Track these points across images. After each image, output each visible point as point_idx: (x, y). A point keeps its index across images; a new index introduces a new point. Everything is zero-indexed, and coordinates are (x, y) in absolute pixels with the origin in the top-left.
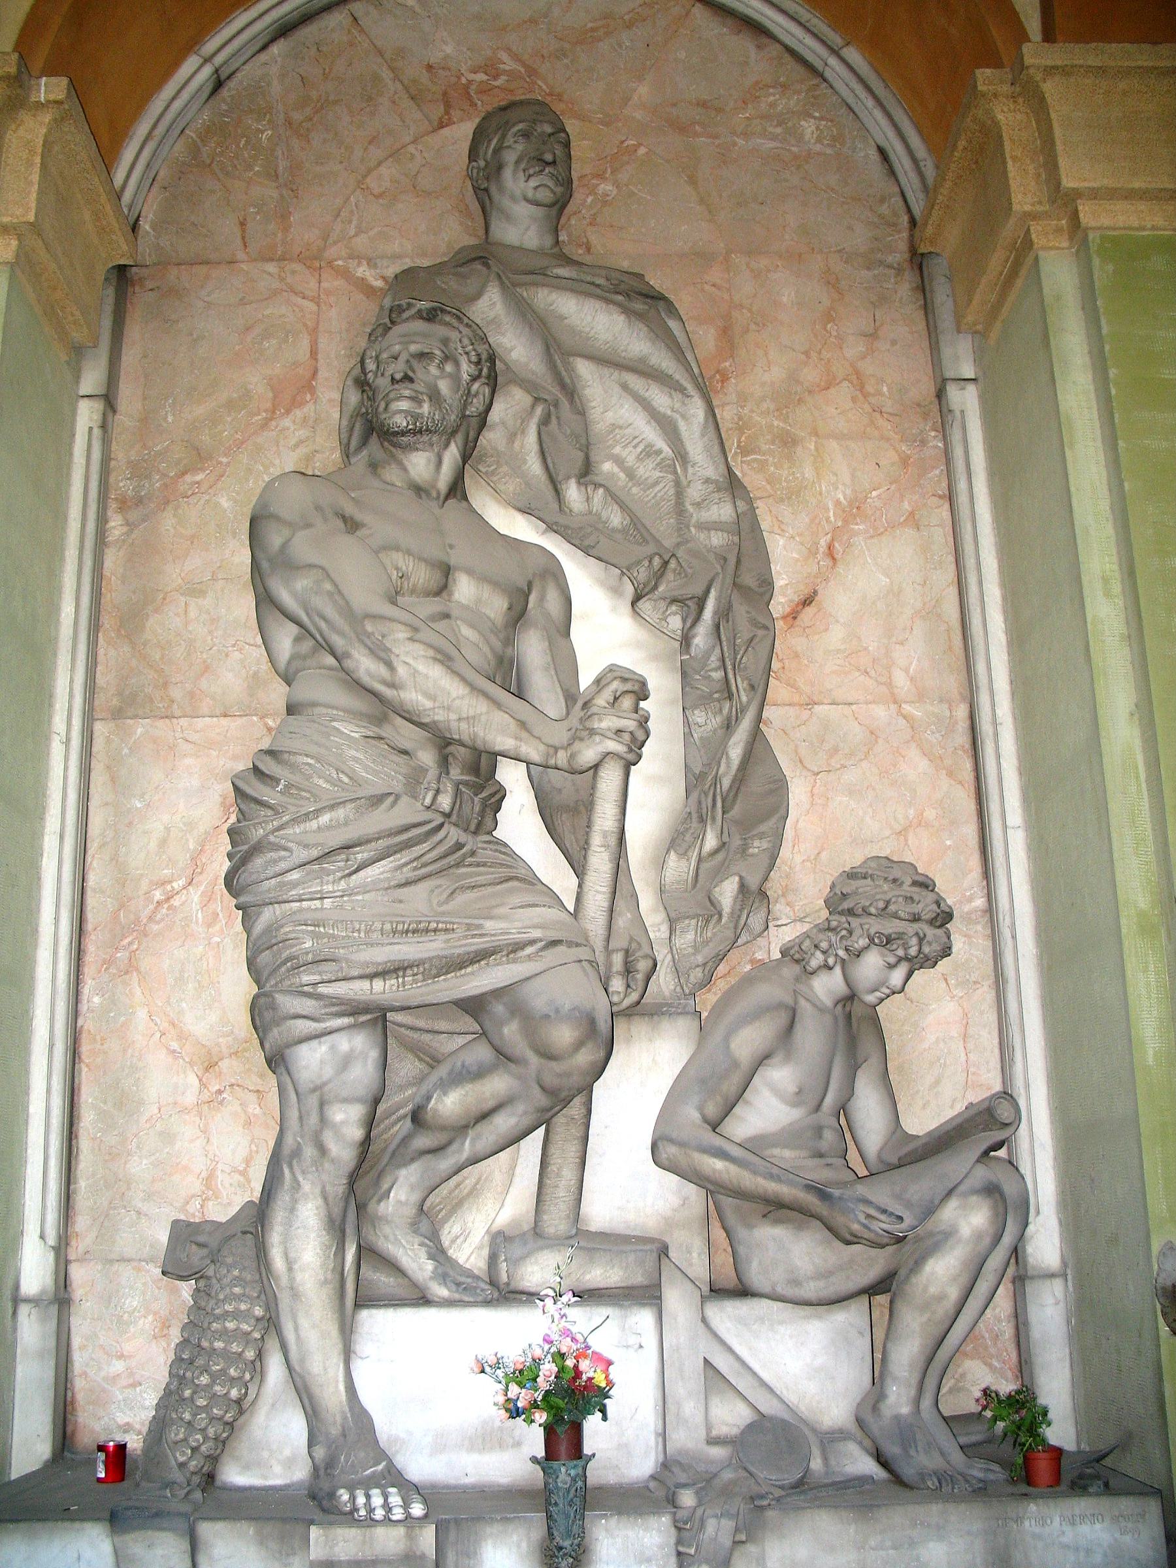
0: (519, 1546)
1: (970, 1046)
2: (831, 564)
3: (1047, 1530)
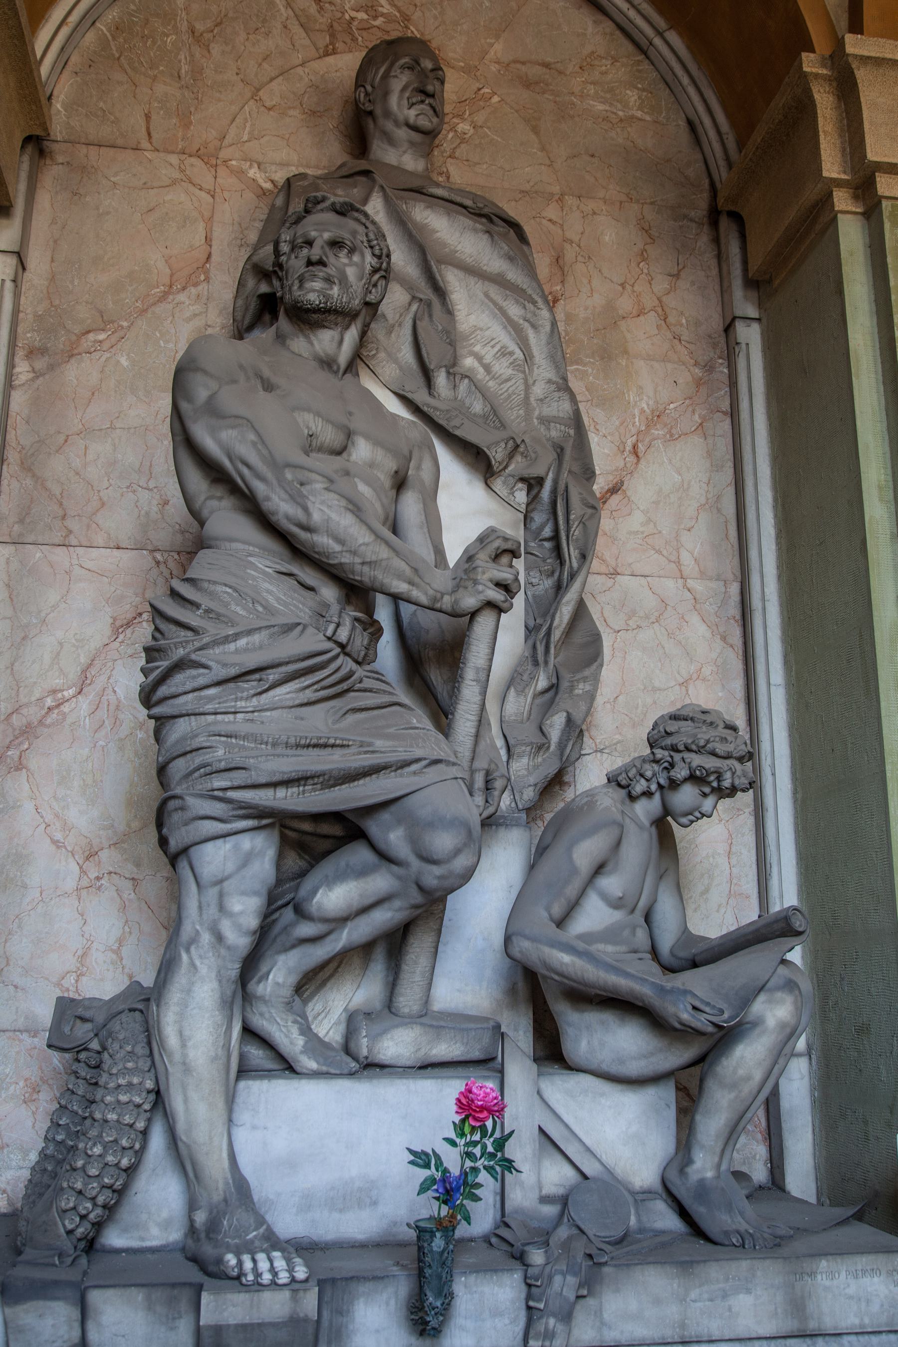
0: (387, 1304)
1: (734, 861)
2: (635, 461)
3: (835, 1282)
